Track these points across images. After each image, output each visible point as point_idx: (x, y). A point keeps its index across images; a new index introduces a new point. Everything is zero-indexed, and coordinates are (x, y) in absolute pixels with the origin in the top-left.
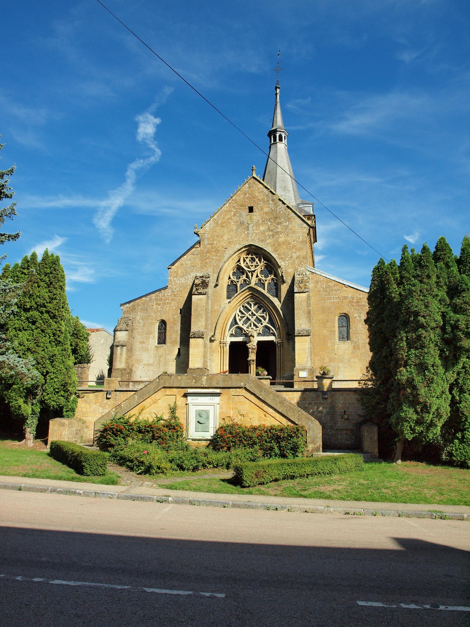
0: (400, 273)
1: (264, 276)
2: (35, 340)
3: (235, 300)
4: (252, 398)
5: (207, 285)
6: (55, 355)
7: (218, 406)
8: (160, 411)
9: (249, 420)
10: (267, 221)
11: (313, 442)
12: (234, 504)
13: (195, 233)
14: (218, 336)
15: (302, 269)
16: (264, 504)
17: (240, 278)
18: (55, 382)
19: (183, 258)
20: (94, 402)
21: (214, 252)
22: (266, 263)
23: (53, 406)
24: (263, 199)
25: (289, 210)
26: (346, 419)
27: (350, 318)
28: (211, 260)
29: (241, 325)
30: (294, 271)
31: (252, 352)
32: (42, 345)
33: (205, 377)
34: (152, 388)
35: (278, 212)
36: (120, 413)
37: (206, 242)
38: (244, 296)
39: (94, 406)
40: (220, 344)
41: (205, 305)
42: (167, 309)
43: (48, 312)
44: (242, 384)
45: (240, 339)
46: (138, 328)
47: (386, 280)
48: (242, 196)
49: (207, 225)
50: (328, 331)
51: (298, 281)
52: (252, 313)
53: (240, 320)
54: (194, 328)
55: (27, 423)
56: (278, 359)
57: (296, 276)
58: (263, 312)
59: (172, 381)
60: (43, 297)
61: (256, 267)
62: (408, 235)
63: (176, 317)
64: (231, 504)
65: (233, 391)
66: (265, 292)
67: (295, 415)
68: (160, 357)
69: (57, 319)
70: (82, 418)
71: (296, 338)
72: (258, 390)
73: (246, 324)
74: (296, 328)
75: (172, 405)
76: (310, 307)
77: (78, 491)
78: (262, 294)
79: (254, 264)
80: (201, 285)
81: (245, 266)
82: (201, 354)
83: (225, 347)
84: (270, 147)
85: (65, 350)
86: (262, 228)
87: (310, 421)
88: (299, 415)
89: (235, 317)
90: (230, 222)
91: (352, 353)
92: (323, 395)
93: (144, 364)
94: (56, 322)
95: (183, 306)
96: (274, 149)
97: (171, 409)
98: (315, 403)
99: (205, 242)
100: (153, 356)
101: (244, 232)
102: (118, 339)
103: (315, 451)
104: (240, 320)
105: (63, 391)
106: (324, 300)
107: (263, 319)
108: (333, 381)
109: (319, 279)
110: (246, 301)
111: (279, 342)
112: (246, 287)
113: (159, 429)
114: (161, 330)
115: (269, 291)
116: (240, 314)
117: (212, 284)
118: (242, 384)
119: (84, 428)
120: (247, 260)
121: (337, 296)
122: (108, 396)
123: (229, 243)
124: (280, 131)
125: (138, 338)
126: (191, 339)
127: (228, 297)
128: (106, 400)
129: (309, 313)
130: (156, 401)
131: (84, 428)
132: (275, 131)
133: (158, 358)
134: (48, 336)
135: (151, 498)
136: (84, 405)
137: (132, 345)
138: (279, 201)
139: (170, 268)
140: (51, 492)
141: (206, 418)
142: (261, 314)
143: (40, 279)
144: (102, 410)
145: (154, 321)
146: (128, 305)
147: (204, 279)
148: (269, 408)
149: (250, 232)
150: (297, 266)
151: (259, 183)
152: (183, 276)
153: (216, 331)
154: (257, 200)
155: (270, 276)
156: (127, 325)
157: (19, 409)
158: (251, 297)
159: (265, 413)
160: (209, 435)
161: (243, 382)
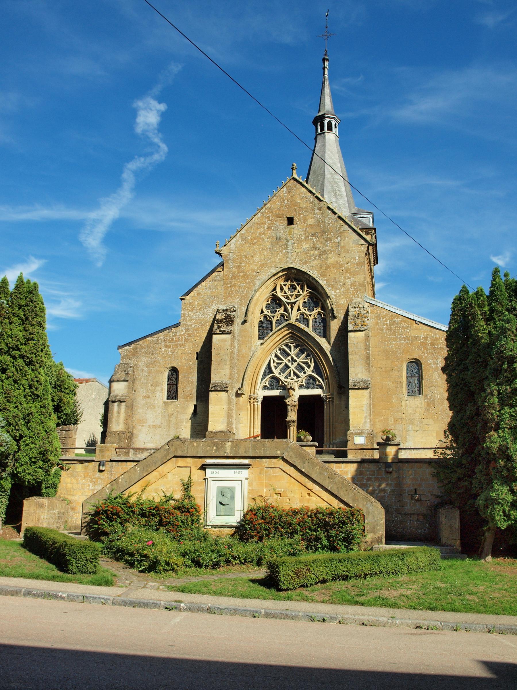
0: (489, 305)
1: (308, 310)
2: (5, 394)
3: (269, 341)
6: (31, 413)
7: (246, 481)
8: (170, 488)
9: (288, 501)
10: (311, 236)
13: (216, 252)
14: (246, 389)
15: (359, 299)
16: (308, 614)
17: (276, 311)
18: (31, 449)
19: (200, 285)
20: (82, 475)
22: (310, 292)
23: (29, 482)
24: (306, 208)
25: (341, 222)
26: (417, 501)
27: (423, 366)
29: (277, 375)
30: (347, 302)
31: (292, 410)
32: (14, 400)
33: (230, 443)
34: (160, 457)
35: (326, 224)
36: (116, 490)
37: (231, 264)
39: (82, 481)
41: (229, 348)
43: (22, 357)
44: (279, 452)
45: (276, 393)
46: (141, 378)
48: (278, 204)
50: (393, 383)
52: (292, 358)
53: (276, 368)
54: (215, 378)
59: (185, 448)
61: (297, 297)
62: (496, 255)
63: (191, 363)
64: (263, 613)
65: (266, 462)
66: (309, 330)
68: (170, 416)
69: (34, 366)
71: (350, 391)
72: (299, 461)
73: (283, 373)
74: (351, 379)
75: (186, 480)
76: (369, 350)
77: (60, 594)
79: (295, 293)
80: (224, 321)
81: (282, 296)
82: (224, 413)
83: (256, 403)
84: (316, 139)
86: (306, 246)
88: (355, 494)
90: (263, 238)
91: (426, 411)
92: (386, 467)
93: (149, 426)
94: (33, 370)
97: (184, 486)
98: (376, 479)
99: (230, 265)
100: (160, 415)
101: (281, 251)
102: (114, 392)
106: (388, 341)
107: (307, 366)
109: (381, 313)
110: (284, 342)
111: (328, 396)
112: (284, 324)
113: (168, 512)
115: (314, 329)
116: (275, 359)
117: (238, 320)
118: (279, 452)
119: (70, 510)
120: (286, 289)
122: (102, 468)
123: (262, 265)
124: (329, 118)
125: (141, 391)
126: (210, 393)
127: (261, 337)
128: (98, 473)
129: (368, 358)
130: (164, 474)
131: (70, 510)
132: (323, 117)
133: (167, 418)
135: (156, 604)
137: (133, 400)
138: (327, 210)
139: (184, 299)
140: (24, 595)
142: (303, 359)
144: (92, 486)
145: (163, 369)
146: (127, 348)
147: (228, 313)
148: (314, 485)
149: (290, 251)
150: (351, 296)
151: (301, 186)
153: (245, 382)
154: (297, 209)
155: (316, 310)
158: (291, 338)
160: (235, 520)
161: (279, 450)
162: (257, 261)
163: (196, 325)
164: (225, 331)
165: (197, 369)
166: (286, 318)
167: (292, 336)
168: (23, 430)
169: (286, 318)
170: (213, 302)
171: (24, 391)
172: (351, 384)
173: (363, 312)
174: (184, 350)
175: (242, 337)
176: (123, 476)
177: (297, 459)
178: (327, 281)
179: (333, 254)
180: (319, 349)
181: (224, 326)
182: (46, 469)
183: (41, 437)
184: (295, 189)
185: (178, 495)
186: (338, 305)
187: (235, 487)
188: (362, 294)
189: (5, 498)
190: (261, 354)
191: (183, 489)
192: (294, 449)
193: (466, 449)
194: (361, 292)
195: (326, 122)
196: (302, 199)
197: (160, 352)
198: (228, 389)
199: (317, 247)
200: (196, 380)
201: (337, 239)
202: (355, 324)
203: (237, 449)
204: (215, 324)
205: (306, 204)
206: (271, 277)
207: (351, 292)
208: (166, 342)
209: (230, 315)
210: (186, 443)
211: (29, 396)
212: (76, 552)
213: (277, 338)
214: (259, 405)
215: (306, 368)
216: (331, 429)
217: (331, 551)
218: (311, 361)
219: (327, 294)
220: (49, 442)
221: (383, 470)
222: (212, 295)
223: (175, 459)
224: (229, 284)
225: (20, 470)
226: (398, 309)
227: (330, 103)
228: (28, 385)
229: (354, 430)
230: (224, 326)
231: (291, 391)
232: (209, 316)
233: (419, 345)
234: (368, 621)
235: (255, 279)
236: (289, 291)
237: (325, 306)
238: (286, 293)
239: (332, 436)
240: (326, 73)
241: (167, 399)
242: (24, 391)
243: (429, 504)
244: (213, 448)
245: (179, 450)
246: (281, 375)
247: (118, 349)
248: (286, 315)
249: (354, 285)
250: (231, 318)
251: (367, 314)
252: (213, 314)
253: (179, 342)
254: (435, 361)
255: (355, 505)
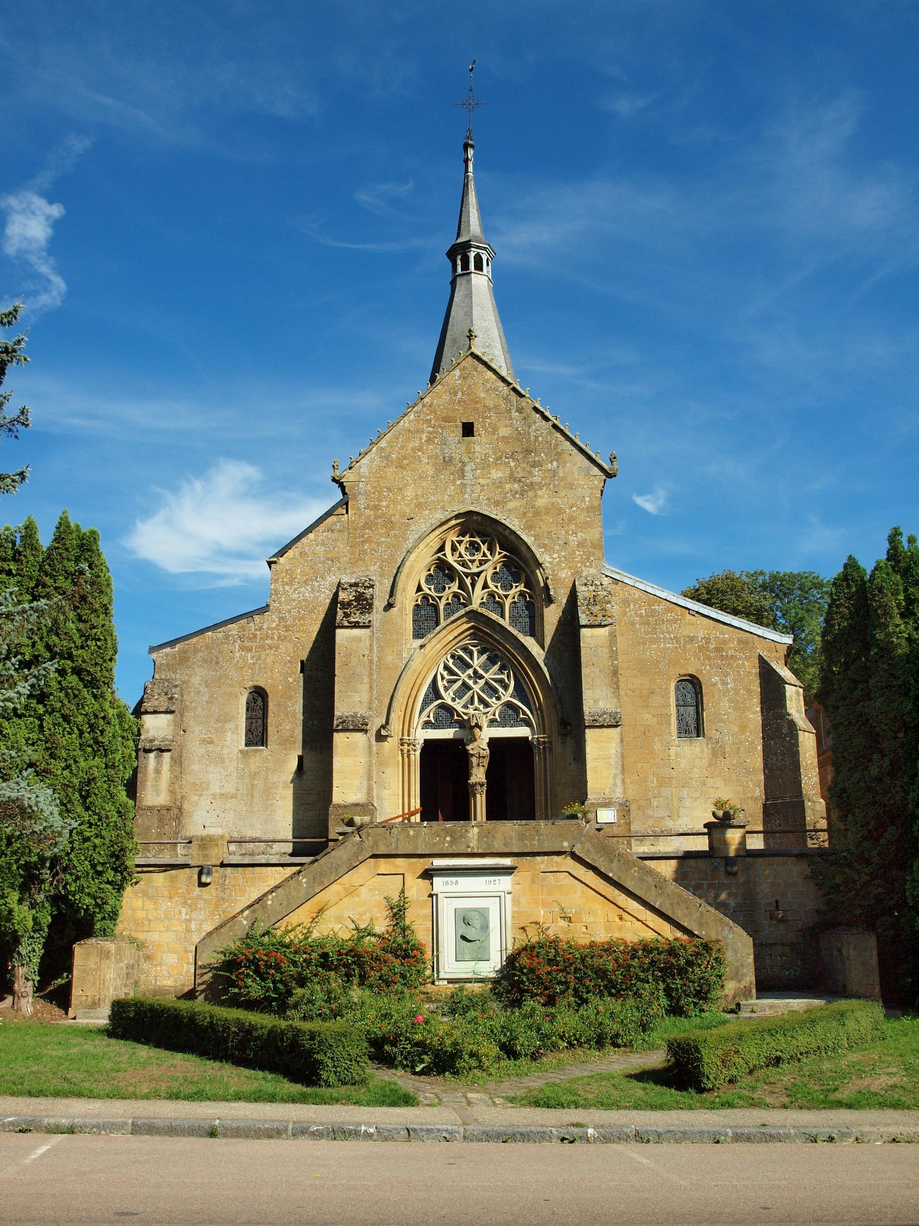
0: (906, 590)
1: (501, 587)
2: (46, 742)
3: (435, 641)
4: (590, 877)
5: (371, 605)
6: (94, 779)
7: (509, 897)
8: (365, 913)
9: (584, 929)
10: (506, 458)
11: (737, 976)
12: (737, 1134)
13: (334, 480)
14: (396, 726)
15: (593, 571)
16: (803, 1130)
17: (444, 589)
18: (95, 847)
19: (306, 538)
20: (166, 893)
21: (382, 526)
22: (505, 556)
23: (87, 910)
24: (496, 407)
25: (558, 435)
26: (781, 921)
27: (703, 687)
28: (374, 546)
29: (449, 701)
30: (572, 574)
31: (478, 765)
32: (64, 754)
33: (476, 830)
34: (345, 857)
35: (532, 438)
36: (262, 921)
37: (362, 501)
38: (456, 633)
39: (166, 905)
40: (402, 745)
41: (367, 653)
42: (269, 660)
43: (77, 671)
44: (566, 844)
45: (447, 734)
46: (196, 708)
47: (879, 607)
48: (446, 397)
49: (364, 461)
50: (654, 716)
51: (585, 599)
52: (475, 672)
53: (446, 689)
54: (342, 708)
55: (19, 954)
56: (540, 781)
57: (580, 589)
58: (501, 670)
59: (393, 840)
60: (66, 634)
61: (481, 564)
62: (641, 493)
63: (291, 680)
64: (730, 1134)
65: (543, 863)
66: (505, 623)
67: (691, 914)
68: (254, 776)
69: (98, 688)
70: (134, 935)
71: (587, 731)
72: (603, 859)
73: (460, 698)
74: (586, 709)
75: (395, 898)
76: (616, 659)
77: (363, 1128)
78: (498, 628)
79: (478, 557)
80: (355, 604)
81: (455, 561)
82: (362, 771)
83: (412, 752)
84: (453, 284)
85: (113, 767)
86: (496, 474)
87: (726, 928)
88: (701, 914)
89: (435, 680)
90: (419, 458)
91: (710, 765)
92: (727, 865)
93: (214, 795)
94: (95, 697)
95: (307, 653)
96: (463, 288)
97: (392, 908)
98: (710, 886)
99: (359, 503)
100: (235, 774)
101: (453, 482)
102: (148, 732)
103: (742, 997)
104: (446, 689)
105: (113, 869)
106: (644, 643)
107: (502, 686)
108: (748, 832)
109: (631, 595)
110: (460, 644)
111: (542, 740)
112: (462, 612)
113: (377, 959)
114: (253, 710)
115: (514, 620)
116: (445, 673)
117: (379, 604)
118: (566, 844)
119: (142, 960)
120: (461, 549)
121: (672, 636)
122: (204, 879)
123: (419, 505)
124: (478, 247)
125: (197, 731)
126: (335, 734)
127: (418, 635)
128: (198, 889)
129: (615, 673)
130: (353, 889)
131: (142, 960)
132: (467, 246)
133: (247, 780)
134: (76, 731)
135: (544, 1133)
136: (139, 903)
137: (181, 747)
138: (534, 413)
139: (275, 562)
140: (294, 1135)
141: (482, 928)
142: (495, 674)
143: (56, 588)
144: (187, 914)
145: (237, 690)
146: (168, 650)
147: (361, 590)
148: (629, 900)
149: (469, 482)
150: (579, 565)
151: (485, 369)
152: (306, 582)
153: (393, 715)
154: (481, 409)
155: (516, 587)
156: (171, 698)
157: (9, 920)
158: (473, 636)
159: (621, 911)
160: (491, 966)
161: (566, 840)
162: (409, 498)
163: (299, 611)
164: (358, 622)
165: (302, 691)
166: (462, 601)
167: (476, 633)
168: (78, 811)
169: (462, 601)
170: (329, 570)
171: (81, 738)
172: (587, 718)
173: (602, 593)
174: (278, 656)
175: (385, 634)
176: (274, 894)
177: (599, 855)
178: (536, 537)
179: (546, 490)
180: (524, 656)
181: (355, 614)
182: (118, 885)
183: (112, 824)
184: (475, 372)
185: (381, 927)
186: (556, 579)
187: (488, 908)
188: (597, 561)
189: (40, 943)
190: (420, 663)
191: (391, 915)
192: (592, 838)
193: (870, 831)
194: (596, 557)
195: (472, 255)
196: (488, 391)
197: (232, 658)
198: (368, 727)
199: (517, 477)
200: (301, 711)
201: (552, 465)
202: (592, 613)
203: (489, 840)
204: (338, 610)
205: (496, 400)
206: (436, 528)
207: (579, 558)
208: (243, 642)
209: (365, 593)
210: (394, 830)
211: (89, 746)
212: (332, 1046)
213: (448, 636)
214: (416, 756)
215: (500, 689)
216: (549, 797)
217: (675, 1015)
218: (508, 677)
219: (537, 560)
220: (127, 834)
221: (722, 869)
222: (328, 556)
223: (373, 860)
224: (359, 537)
225: (73, 889)
226: (660, 588)
227: (478, 223)
228: (88, 726)
229: (595, 799)
230: (355, 614)
231: (477, 730)
232: (323, 595)
233: (695, 651)
234: (901, 1134)
235: (406, 530)
236: (468, 554)
237: (533, 580)
238: (487, 557)
239: (551, 810)
240: (471, 169)
241: (246, 745)
242: (81, 738)
243: (800, 927)
244: (445, 838)
245: (381, 844)
246: (456, 703)
247: (150, 652)
248: (461, 594)
249: (583, 546)
250: (366, 599)
251: (610, 597)
252: (331, 590)
253: (268, 642)
254: (723, 678)
255: (704, 933)
